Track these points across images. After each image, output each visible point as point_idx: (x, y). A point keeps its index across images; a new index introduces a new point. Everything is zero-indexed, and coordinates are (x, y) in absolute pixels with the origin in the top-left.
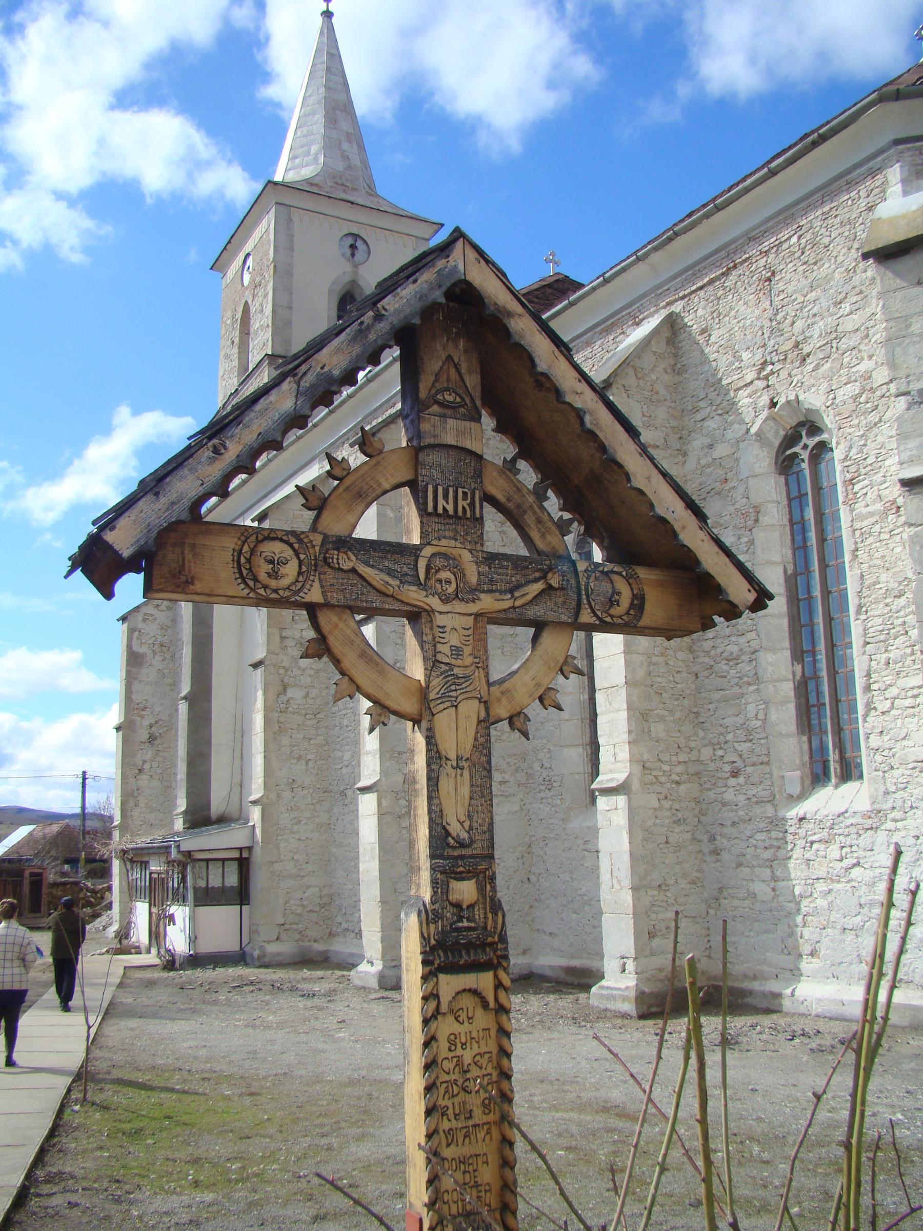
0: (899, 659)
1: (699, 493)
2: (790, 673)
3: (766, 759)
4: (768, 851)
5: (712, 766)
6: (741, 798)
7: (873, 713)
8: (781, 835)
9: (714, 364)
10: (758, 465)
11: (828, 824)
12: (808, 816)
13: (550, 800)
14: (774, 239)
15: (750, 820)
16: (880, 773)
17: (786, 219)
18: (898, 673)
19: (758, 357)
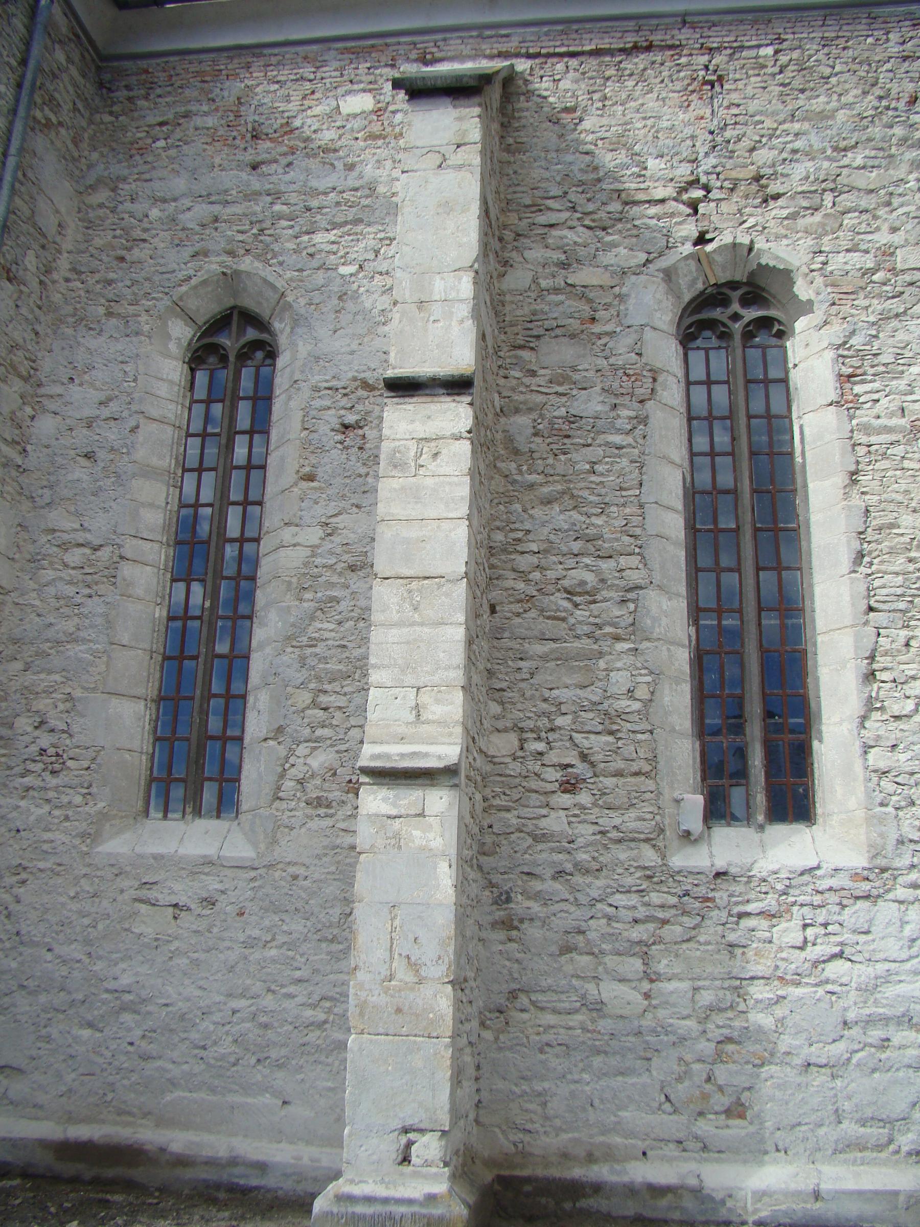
1: (529, 325)
3: (647, 768)
4: (640, 927)
10: (658, 315)
11: (779, 887)
13: (51, 794)
16: (890, 809)
17: (756, 22)
19: (683, 171)
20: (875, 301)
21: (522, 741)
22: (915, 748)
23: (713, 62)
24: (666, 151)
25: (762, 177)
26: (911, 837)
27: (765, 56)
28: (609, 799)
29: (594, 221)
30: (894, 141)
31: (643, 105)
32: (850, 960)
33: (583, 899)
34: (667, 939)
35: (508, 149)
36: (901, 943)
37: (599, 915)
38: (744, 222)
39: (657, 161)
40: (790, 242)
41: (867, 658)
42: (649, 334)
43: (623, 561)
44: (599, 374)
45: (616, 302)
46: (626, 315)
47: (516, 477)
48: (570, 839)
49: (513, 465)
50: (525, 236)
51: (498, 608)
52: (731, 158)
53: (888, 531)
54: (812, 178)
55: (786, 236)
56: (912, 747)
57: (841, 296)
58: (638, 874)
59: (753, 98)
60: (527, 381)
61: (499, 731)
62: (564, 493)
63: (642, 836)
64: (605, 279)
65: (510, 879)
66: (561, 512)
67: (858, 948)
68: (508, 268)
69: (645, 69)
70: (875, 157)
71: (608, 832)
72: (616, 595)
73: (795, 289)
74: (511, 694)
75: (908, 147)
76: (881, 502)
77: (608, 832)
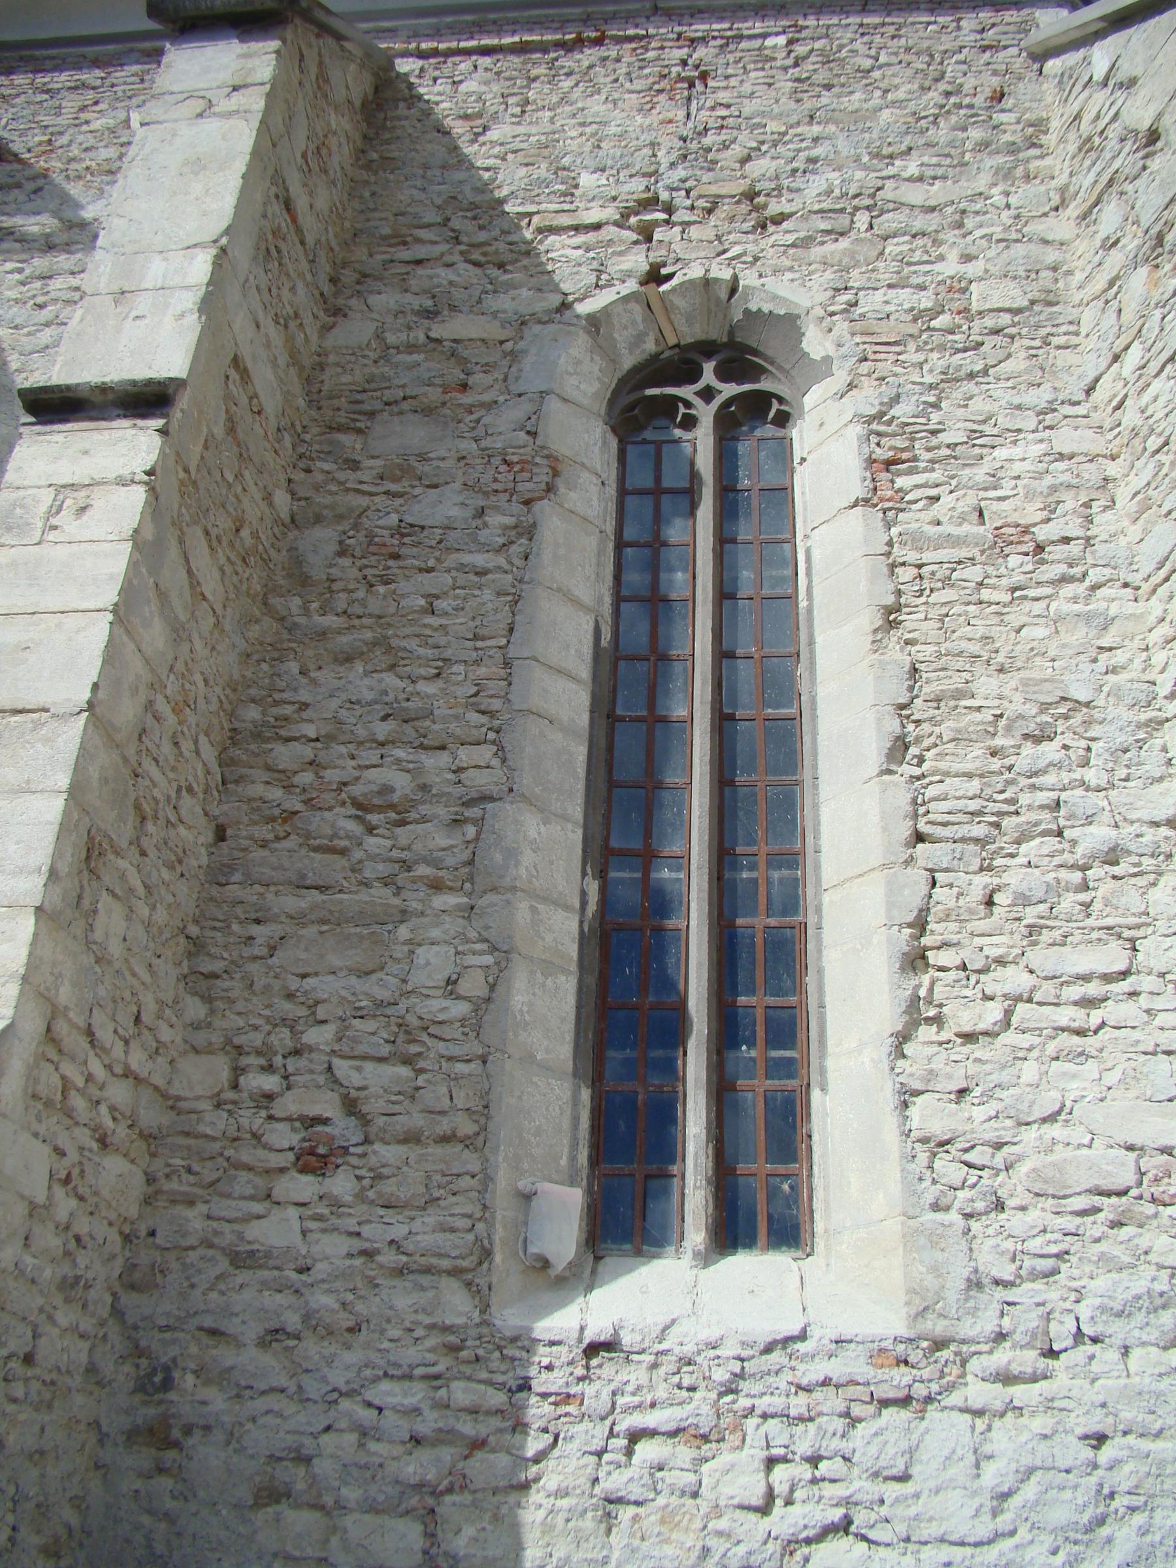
0: (1039, 894)
2: (577, 892)
3: (467, 1127)
4: (425, 1454)
5: (216, 1123)
6: (332, 1249)
7: (926, 1032)
8: (498, 1398)
9: (486, 175)
11: (720, 1375)
12: (627, 1339)
14: (726, 25)
15: (354, 1330)
16: (954, 1216)
18: (1033, 930)
20: (935, 355)
21: (238, 1071)
22: (1004, 1094)
23: (695, 56)
24: (609, 163)
25: (758, 194)
26: (996, 1273)
27: (775, 46)
28: (388, 1187)
29: (484, 254)
30: (969, 145)
31: (583, 109)
32: (864, 1538)
33: (314, 1389)
34: (479, 1483)
35: (368, 166)
36: (976, 1502)
37: (343, 1424)
38: (724, 252)
39: (596, 176)
40: (797, 276)
41: (910, 925)
42: (553, 405)
43: (465, 755)
44: (462, 463)
45: (505, 362)
46: (517, 379)
47: (297, 619)
48: (301, 1262)
49: (297, 601)
50: (377, 279)
51: (229, 832)
52: (710, 170)
53: (952, 703)
54: (837, 192)
55: (791, 269)
56: (999, 1093)
57: (878, 348)
58: (431, 1342)
59: (751, 96)
60: (341, 476)
61: (197, 1051)
62: (375, 644)
63: (445, 1264)
64: (494, 331)
65: (174, 1341)
66: (367, 674)
67: (884, 1511)
68: (340, 319)
69: (591, 67)
70: (939, 165)
71: (378, 1252)
72: (442, 812)
73: (804, 345)
74: (227, 984)
75: (990, 154)
76: (940, 655)
77: (378, 1252)
